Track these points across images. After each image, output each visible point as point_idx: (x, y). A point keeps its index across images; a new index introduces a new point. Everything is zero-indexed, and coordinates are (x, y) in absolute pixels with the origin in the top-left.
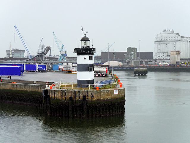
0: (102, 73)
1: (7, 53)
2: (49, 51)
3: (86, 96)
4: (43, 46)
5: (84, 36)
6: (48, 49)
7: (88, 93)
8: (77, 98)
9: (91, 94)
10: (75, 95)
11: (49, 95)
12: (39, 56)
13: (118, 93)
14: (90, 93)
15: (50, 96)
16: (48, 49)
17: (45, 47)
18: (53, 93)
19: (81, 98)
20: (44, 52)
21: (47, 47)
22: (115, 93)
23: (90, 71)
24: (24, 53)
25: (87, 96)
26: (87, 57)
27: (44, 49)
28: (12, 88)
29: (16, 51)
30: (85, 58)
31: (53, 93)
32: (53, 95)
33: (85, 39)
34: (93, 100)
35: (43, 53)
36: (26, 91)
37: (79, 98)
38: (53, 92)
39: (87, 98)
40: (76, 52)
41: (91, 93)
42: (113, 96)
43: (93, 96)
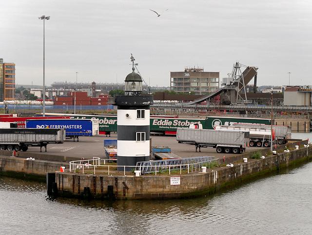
0: (255, 139)
1: (172, 79)
2: (254, 78)
3: (112, 186)
4: (237, 66)
5: (131, 71)
6: (251, 73)
7: (117, 182)
8: (98, 189)
9: (124, 183)
10: (95, 185)
11: (56, 183)
12: (225, 91)
13: (179, 183)
14: (120, 182)
15: (58, 186)
16: (251, 73)
17: (243, 69)
18: (61, 178)
19: (104, 190)
20: (239, 81)
21: (248, 68)
22: (172, 183)
23: (139, 140)
24: (217, 81)
25: (115, 186)
26: (133, 113)
27: (239, 73)
28: (25, 170)
29: (196, 73)
30: (127, 115)
31: (61, 178)
32: (61, 184)
33: (133, 78)
34: (126, 194)
35: (236, 84)
36: (15, 170)
37: (102, 190)
38: (61, 176)
39: (115, 190)
40: (114, 103)
41: (122, 181)
42: (167, 188)
43: (126, 187)
